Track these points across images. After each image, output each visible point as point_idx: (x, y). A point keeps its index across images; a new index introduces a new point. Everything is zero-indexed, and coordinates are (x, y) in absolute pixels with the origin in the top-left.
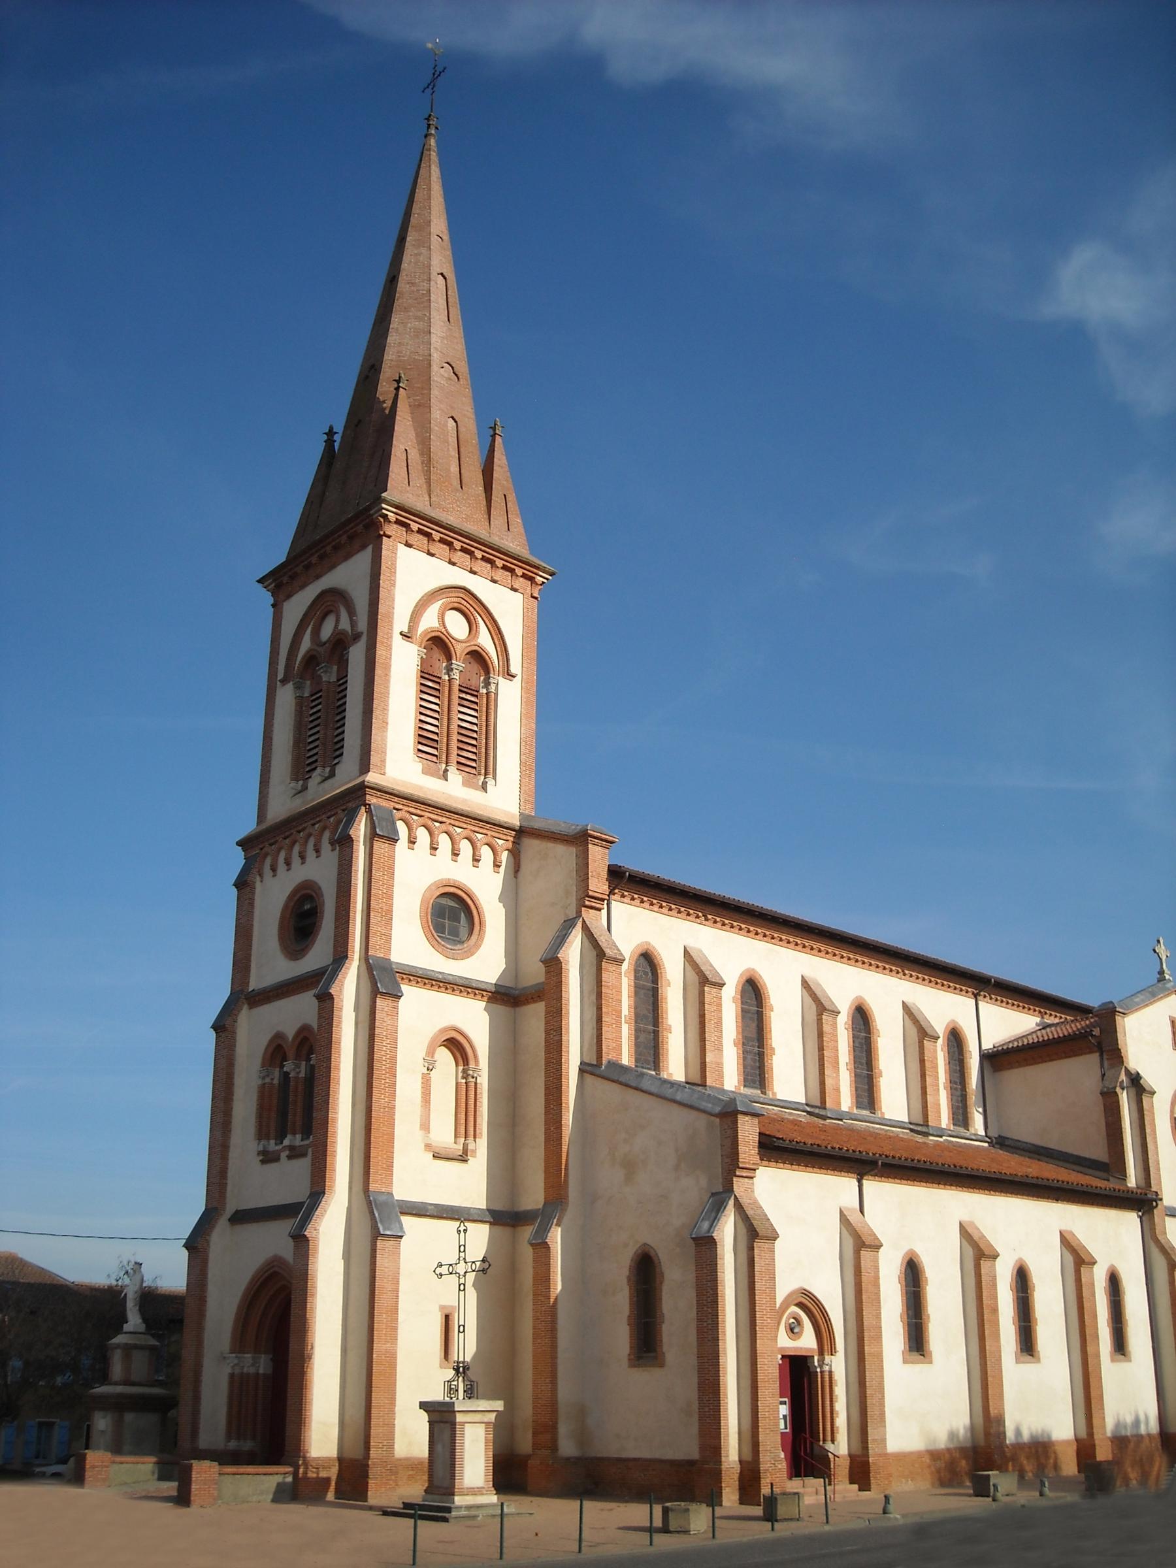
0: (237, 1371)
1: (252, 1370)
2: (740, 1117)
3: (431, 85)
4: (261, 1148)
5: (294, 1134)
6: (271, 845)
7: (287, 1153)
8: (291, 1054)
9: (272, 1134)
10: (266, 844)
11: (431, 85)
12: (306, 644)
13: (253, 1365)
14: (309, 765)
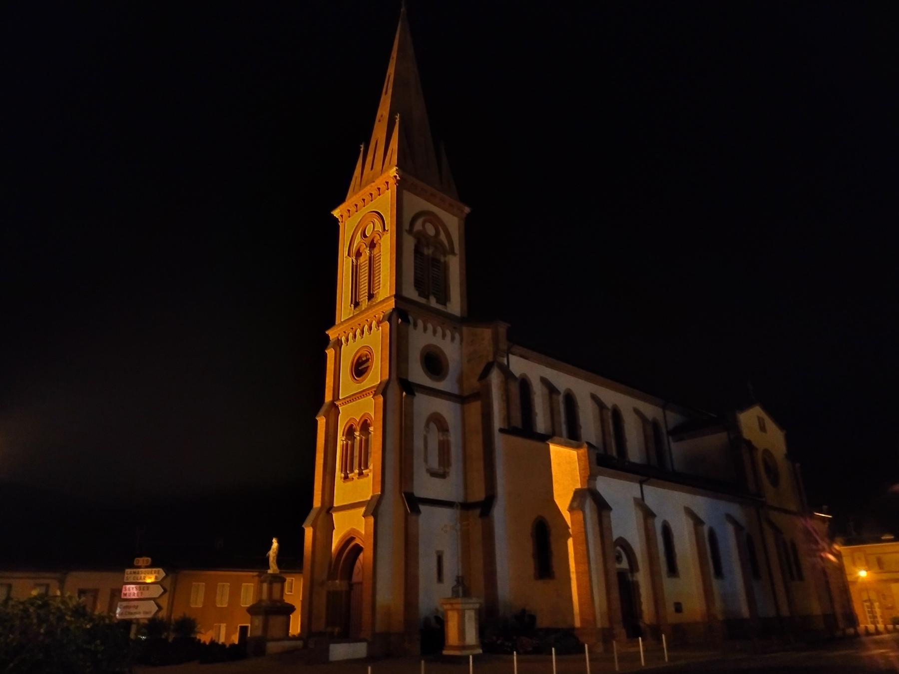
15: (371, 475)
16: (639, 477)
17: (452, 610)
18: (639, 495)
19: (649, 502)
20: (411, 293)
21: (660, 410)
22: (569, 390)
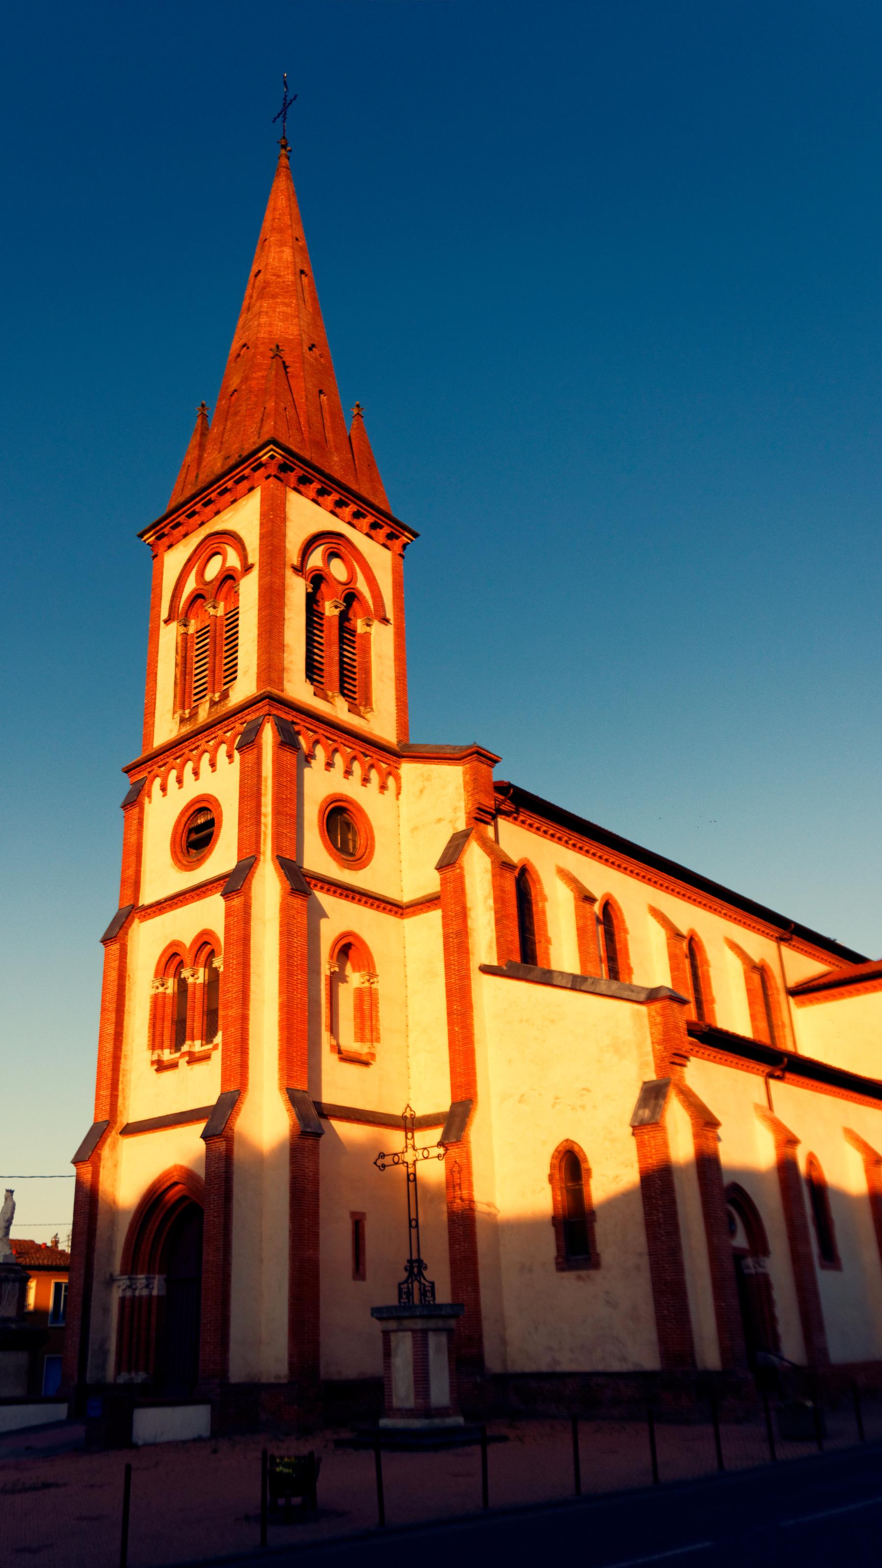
0: (129, 1293)
1: (145, 1292)
2: (477, 1449)
3: (283, 113)
4: (155, 1058)
5: (193, 1040)
6: (160, 767)
7: (187, 1058)
8: (188, 959)
9: (167, 1042)
10: (155, 767)
11: (283, 113)
12: (191, 585)
13: (147, 1286)
14: (196, 694)
15: (217, 1056)
16: (767, 1069)
17: (436, 1330)
18: (764, 1102)
19: (783, 1113)
20: (298, 688)
21: (773, 945)
22: (611, 895)
